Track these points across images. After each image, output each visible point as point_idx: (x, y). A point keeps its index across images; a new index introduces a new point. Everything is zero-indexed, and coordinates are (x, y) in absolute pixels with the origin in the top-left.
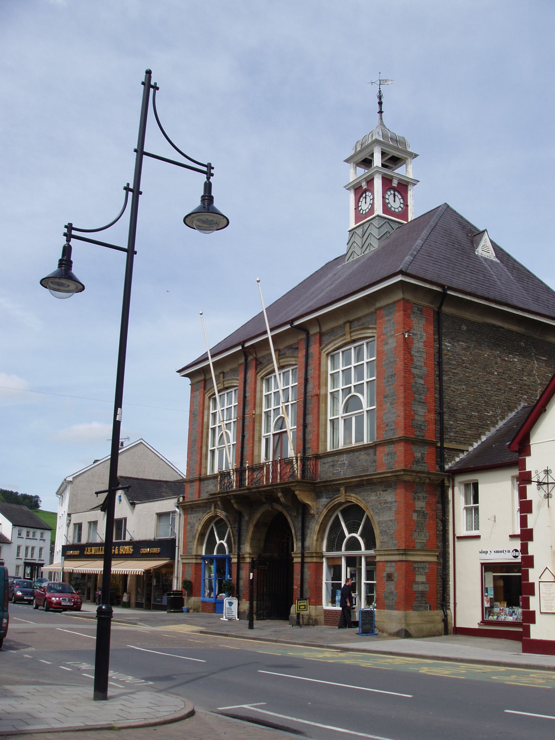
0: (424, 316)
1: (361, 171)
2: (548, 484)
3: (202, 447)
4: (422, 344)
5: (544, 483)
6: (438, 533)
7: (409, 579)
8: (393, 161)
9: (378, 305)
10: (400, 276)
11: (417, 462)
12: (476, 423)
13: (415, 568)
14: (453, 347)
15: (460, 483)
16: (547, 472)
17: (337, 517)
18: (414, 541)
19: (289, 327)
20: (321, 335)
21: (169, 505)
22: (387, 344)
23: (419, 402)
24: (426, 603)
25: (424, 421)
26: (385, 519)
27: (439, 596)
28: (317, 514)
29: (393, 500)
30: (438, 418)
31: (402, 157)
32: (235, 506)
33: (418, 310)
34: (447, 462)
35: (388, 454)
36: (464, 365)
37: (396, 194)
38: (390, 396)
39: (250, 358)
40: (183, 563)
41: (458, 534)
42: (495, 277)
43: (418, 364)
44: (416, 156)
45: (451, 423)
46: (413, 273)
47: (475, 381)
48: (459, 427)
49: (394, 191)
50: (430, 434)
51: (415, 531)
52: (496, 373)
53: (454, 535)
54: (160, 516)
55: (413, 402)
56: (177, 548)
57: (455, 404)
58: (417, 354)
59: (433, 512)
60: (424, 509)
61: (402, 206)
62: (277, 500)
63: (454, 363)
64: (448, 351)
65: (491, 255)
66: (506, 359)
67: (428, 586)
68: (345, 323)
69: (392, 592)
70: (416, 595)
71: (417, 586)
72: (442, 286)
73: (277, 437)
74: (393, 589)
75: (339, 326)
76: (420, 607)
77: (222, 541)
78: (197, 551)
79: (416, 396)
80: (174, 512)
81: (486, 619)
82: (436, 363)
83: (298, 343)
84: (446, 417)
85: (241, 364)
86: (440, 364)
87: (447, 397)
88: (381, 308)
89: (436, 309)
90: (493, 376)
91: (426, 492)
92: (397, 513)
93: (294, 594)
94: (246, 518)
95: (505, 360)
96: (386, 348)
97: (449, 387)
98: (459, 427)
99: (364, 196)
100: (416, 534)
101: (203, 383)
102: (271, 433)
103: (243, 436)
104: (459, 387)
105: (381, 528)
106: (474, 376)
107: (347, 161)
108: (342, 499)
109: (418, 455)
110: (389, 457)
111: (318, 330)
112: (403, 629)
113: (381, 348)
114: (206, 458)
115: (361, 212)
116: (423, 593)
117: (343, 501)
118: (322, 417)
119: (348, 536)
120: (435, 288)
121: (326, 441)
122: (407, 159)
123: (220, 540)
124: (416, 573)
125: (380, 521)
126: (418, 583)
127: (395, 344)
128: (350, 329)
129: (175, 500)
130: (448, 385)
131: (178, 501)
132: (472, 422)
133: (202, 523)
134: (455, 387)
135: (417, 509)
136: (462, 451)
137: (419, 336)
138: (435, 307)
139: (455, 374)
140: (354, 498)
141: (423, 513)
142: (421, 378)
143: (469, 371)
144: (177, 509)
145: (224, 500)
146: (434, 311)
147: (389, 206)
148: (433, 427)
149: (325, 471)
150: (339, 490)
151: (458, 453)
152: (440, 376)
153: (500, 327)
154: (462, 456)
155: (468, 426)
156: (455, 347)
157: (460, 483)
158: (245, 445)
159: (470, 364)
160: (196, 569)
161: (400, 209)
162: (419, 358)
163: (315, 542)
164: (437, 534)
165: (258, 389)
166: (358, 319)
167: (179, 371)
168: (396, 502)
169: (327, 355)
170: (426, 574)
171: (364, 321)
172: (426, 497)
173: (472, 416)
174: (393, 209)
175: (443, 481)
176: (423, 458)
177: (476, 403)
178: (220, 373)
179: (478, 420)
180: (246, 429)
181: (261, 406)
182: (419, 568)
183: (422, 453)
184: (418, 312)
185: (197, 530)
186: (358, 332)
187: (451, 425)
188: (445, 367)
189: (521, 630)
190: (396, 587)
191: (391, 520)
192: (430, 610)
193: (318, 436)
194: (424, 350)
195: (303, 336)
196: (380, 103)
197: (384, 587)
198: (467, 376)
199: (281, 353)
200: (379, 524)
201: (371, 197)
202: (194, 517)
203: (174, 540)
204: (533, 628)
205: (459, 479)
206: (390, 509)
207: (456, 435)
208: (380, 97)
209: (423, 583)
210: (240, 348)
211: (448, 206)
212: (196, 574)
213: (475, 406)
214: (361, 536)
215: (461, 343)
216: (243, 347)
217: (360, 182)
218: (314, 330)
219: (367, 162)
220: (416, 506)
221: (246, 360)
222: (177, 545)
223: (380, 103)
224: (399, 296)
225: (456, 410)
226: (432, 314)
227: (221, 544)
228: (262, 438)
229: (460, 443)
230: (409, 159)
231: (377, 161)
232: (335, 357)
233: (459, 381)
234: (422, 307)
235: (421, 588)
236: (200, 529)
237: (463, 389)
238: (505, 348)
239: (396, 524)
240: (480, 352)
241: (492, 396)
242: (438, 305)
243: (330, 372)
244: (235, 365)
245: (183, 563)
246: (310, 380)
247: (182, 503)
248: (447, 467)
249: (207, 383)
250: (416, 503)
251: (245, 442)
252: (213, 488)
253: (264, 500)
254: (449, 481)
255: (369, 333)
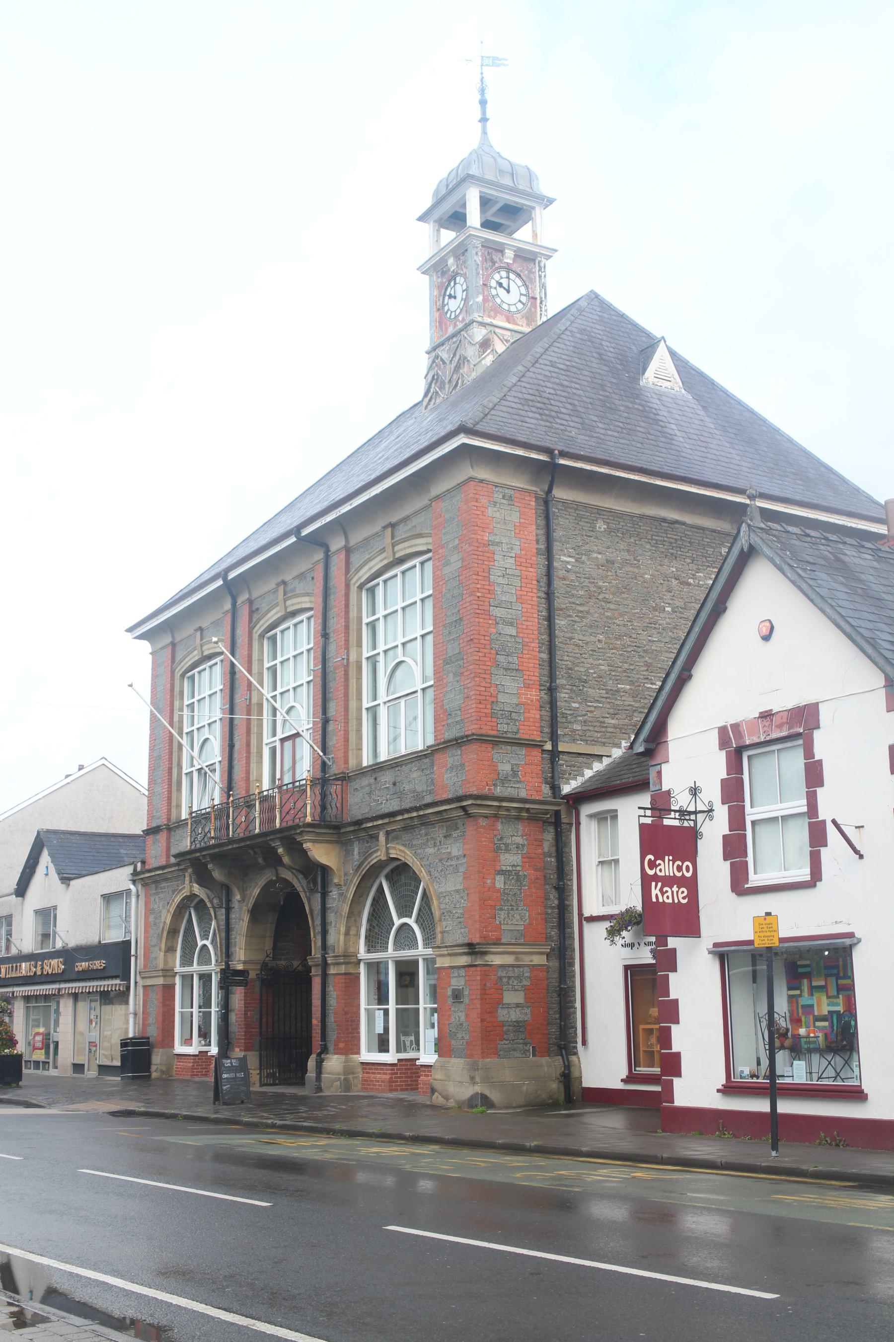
0: (518, 509)
1: (448, 236)
2: (695, 813)
3: (170, 769)
4: (512, 561)
5: (690, 813)
6: (549, 911)
7: (490, 1001)
8: (506, 214)
9: (435, 491)
10: (462, 435)
11: (504, 781)
12: (627, 703)
13: (501, 978)
14: (577, 564)
15: (591, 816)
16: (694, 791)
17: (381, 889)
18: (499, 927)
19: (293, 539)
20: (348, 551)
21: (119, 878)
22: (448, 564)
23: (506, 669)
24: (526, 1044)
25: (517, 705)
26: (449, 889)
27: (554, 1029)
28: (345, 885)
29: (460, 853)
30: (546, 698)
31: (523, 205)
32: (217, 875)
33: (504, 497)
34: (568, 779)
35: (452, 768)
36: (600, 597)
37: (512, 276)
38: (453, 659)
39: (243, 598)
40: (144, 987)
41: (587, 913)
42: (674, 427)
43: (504, 598)
44: (551, 201)
45: (574, 705)
46: (492, 430)
47: (624, 625)
48: (591, 712)
49: (508, 273)
50: (531, 725)
51: (501, 910)
52: (669, 609)
53: (580, 914)
54: (108, 898)
55: (494, 670)
56: (133, 959)
57: (582, 669)
58: (501, 580)
59: (539, 873)
60: (519, 868)
61: (524, 299)
62: (278, 861)
63: (581, 593)
64: (568, 571)
65: (673, 384)
66: (691, 581)
67: (528, 1011)
68: (385, 528)
69: (461, 1024)
70: (505, 1028)
71: (505, 1012)
72: (549, 451)
73: (288, 744)
74: (463, 1018)
75: (376, 535)
76: (514, 1050)
77: (205, 942)
78: (166, 961)
79: (501, 658)
80: (129, 891)
81: (643, 1070)
82: (543, 595)
83: (311, 570)
84: (562, 695)
85: (226, 613)
86: (549, 596)
87: (566, 658)
88: (438, 498)
89: (542, 494)
90: (662, 615)
91: (522, 836)
92: (466, 877)
93: (314, 1035)
94: (238, 897)
95: (689, 584)
96: (447, 570)
97: (571, 639)
98: (591, 712)
99: (452, 284)
100: (503, 914)
101: (170, 649)
102: (277, 738)
103: (231, 746)
104: (592, 638)
105: (443, 906)
106: (621, 615)
107: (421, 219)
108: (380, 855)
109: (505, 768)
110: (454, 774)
111: (343, 543)
112: (478, 1093)
113: (439, 572)
114: (179, 789)
115: (448, 315)
116: (518, 1026)
117: (383, 858)
118: (353, 704)
119: (397, 922)
120: (534, 455)
121: (360, 749)
122: (533, 208)
123: (202, 939)
124: (505, 988)
125: (442, 893)
126: (508, 1006)
127: (459, 564)
128: (393, 538)
129: (129, 870)
130: (567, 635)
131: (135, 869)
132: (618, 703)
133: (172, 910)
134: (581, 637)
135: (504, 868)
136: (599, 757)
137: (505, 547)
138: (539, 490)
139: (582, 615)
140: (399, 851)
141: (517, 874)
142: (511, 624)
143: (612, 606)
144: (132, 887)
145: (196, 863)
146: (536, 497)
147: (498, 301)
148: (535, 714)
149: (359, 803)
150: (376, 838)
151: (589, 761)
152: (550, 619)
153: (677, 522)
154: (598, 766)
155: (611, 711)
156: (583, 563)
157: (591, 816)
158: (235, 762)
159: (614, 594)
160: (164, 997)
161: (520, 306)
162: (506, 588)
163: (342, 938)
164: (547, 914)
165: (255, 656)
166: (405, 519)
167: (130, 630)
168: (465, 856)
169: (361, 587)
170: (526, 989)
171: (414, 522)
172: (523, 845)
173: (618, 691)
174: (505, 307)
175: (557, 814)
176: (515, 773)
177: (626, 666)
178: (196, 630)
179: (631, 699)
180: (236, 733)
181: (359, 645)
182: (509, 978)
183: (512, 765)
184: (504, 501)
185: (165, 922)
186: (406, 544)
187: (576, 709)
188: (559, 602)
189: (658, 1088)
190: (467, 1016)
191: (457, 891)
192: (534, 1055)
193: (347, 740)
194: (517, 573)
195: (320, 556)
196: (483, 103)
197: (449, 1016)
198: (607, 617)
199: (288, 589)
200: (439, 898)
201: (464, 287)
202: (160, 899)
203: (128, 943)
204: (678, 1083)
205: (587, 810)
206: (456, 869)
207: (585, 728)
208: (482, 91)
209: (518, 1005)
210: (220, 582)
211: (597, 296)
212: (164, 1005)
213: (625, 671)
214: (212, 943)
215: (595, 555)
216: (225, 580)
217: (443, 260)
218: (337, 544)
219: (457, 219)
220: (503, 863)
221: (234, 604)
222: (133, 952)
223: (483, 103)
224: (466, 471)
225: (585, 681)
226: (533, 503)
227: (204, 946)
228: (264, 746)
229: (595, 742)
230: (538, 210)
231: (474, 217)
232: (376, 590)
233: (591, 627)
234: (512, 492)
235: (514, 1015)
236: (168, 921)
237: (599, 641)
238: (689, 561)
239: (465, 898)
240: (636, 570)
241: (661, 652)
242: (546, 488)
243: (365, 620)
244: (217, 615)
245: (144, 987)
246: (333, 637)
247: (142, 872)
248: (566, 789)
249: (177, 648)
250: (502, 857)
251: (236, 755)
252: (184, 843)
253: (260, 860)
254: (569, 813)
255: (420, 544)
